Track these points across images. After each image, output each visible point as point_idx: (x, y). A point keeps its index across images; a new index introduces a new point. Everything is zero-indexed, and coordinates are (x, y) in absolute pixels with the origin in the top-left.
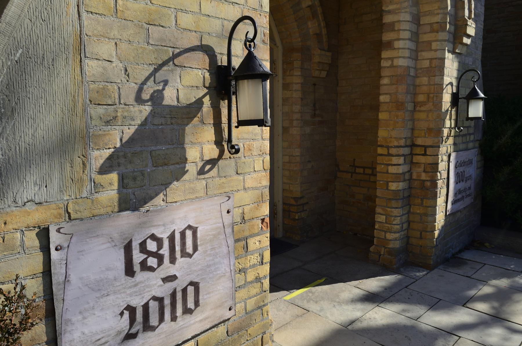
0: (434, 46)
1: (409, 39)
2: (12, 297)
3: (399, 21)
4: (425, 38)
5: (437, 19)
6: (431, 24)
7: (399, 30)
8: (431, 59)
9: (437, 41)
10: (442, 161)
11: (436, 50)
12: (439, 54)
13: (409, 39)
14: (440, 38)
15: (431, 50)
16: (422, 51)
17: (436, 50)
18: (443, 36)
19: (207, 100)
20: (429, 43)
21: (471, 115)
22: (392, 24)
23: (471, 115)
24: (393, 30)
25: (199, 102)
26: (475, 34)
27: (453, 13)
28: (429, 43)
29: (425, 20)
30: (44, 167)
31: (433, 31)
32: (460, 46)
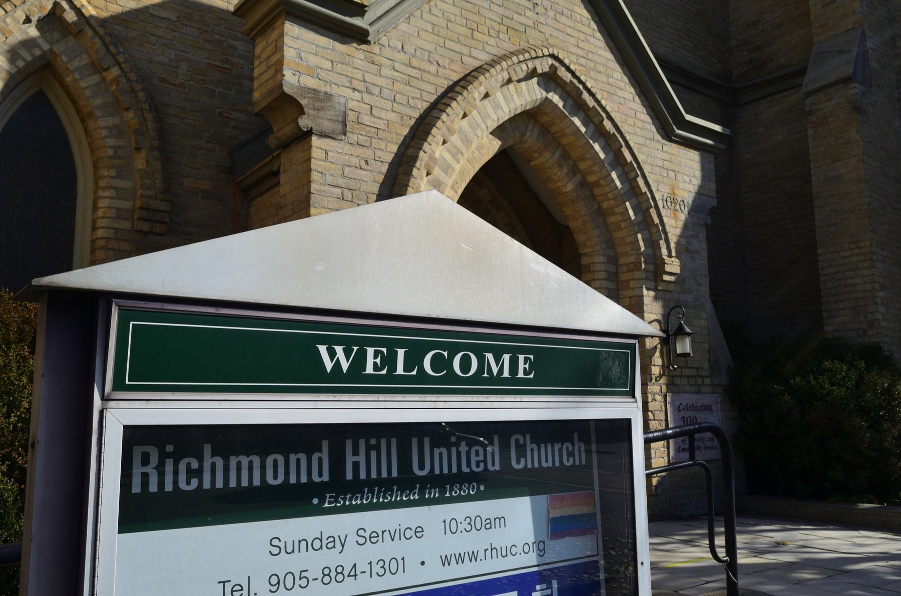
0: (632, 284)
1: (605, 279)
2: (9, 348)
3: (594, 263)
4: (624, 277)
5: (632, 259)
6: (627, 264)
7: (595, 271)
8: (630, 297)
9: (633, 279)
10: (654, 400)
11: (633, 289)
12: (636, 292)
13: (605, 279)
14: (636, 277)
15: (630, 288)
16: (623, 289)
17: (633, 289)
18: (637, 275)
19: (659, 346)
20: (628, 281)
21: (679, 351)
22: (588, 266)
23: (679, 351)
24: (590, 272)
25: (655, 347)
26: (681, 270)
27: (649, 251)
28: (628, 281)
29: (622, 260)
30: (550, 453)
31: (629, 271)
32: (661, 283)
